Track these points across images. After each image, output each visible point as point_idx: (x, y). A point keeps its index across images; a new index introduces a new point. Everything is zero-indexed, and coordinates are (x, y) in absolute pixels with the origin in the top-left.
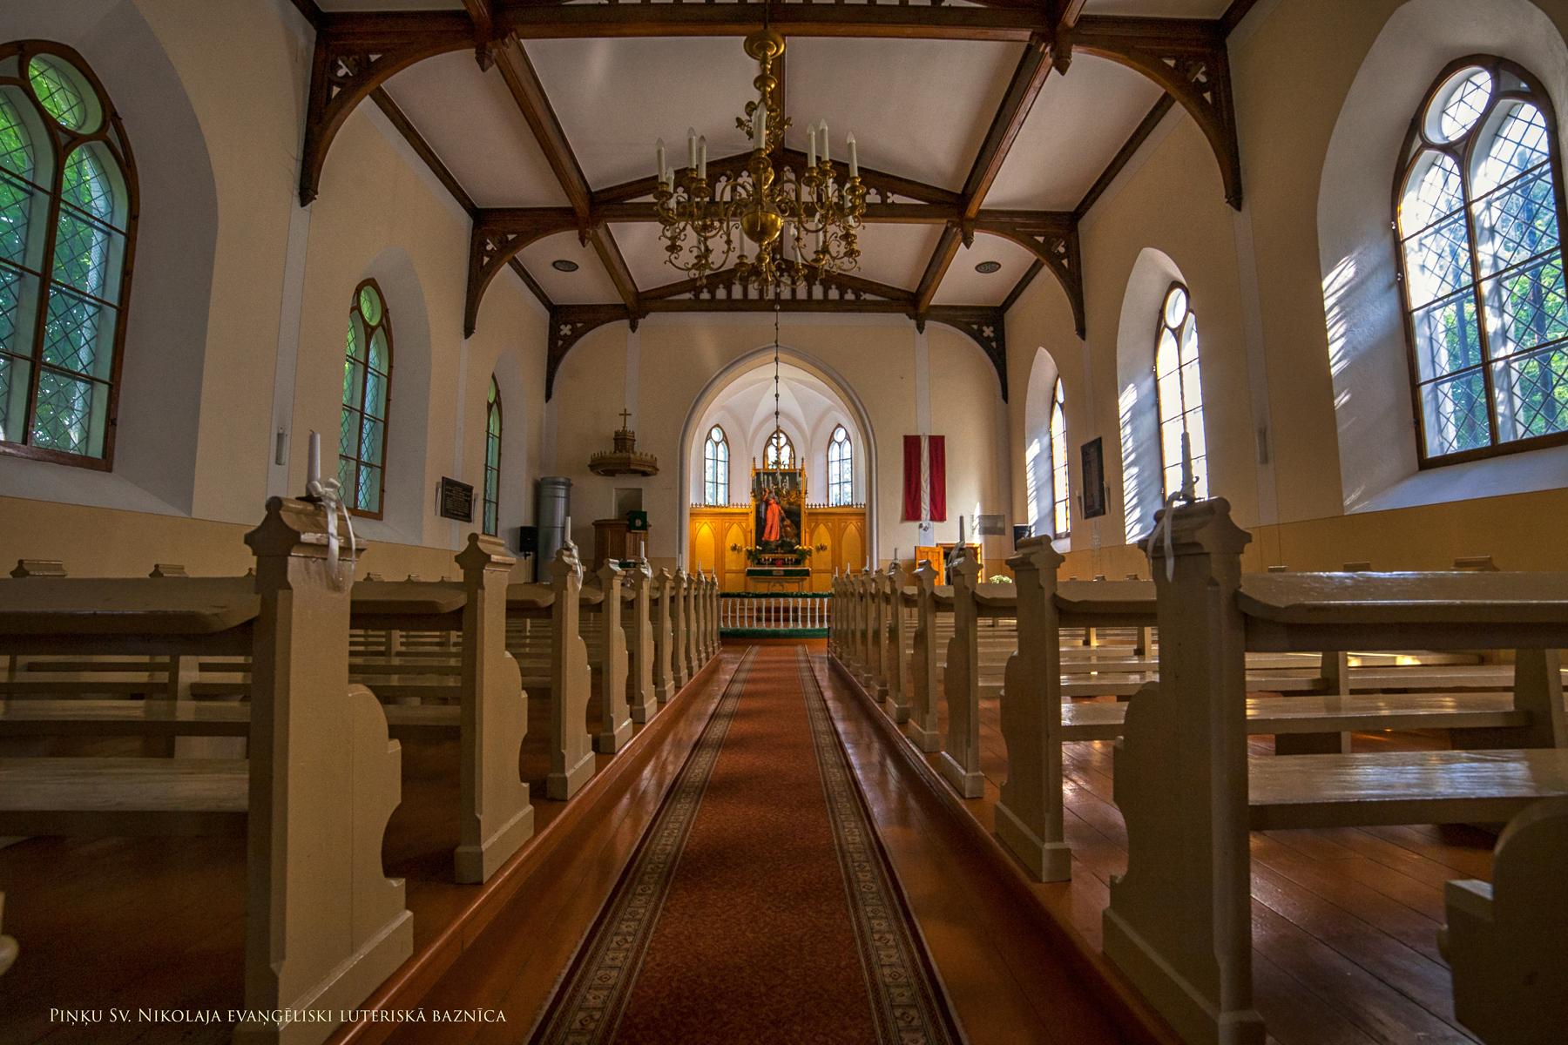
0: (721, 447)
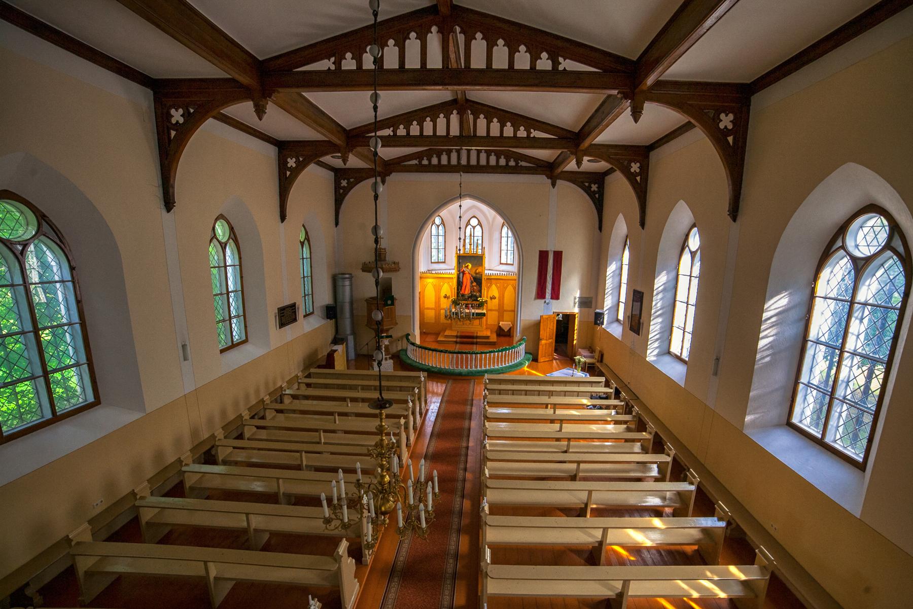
0: (440, 227)
